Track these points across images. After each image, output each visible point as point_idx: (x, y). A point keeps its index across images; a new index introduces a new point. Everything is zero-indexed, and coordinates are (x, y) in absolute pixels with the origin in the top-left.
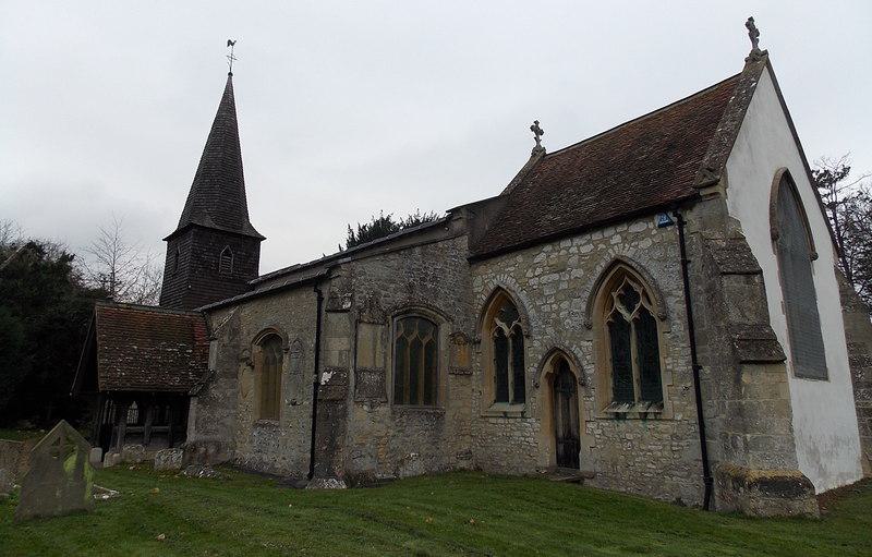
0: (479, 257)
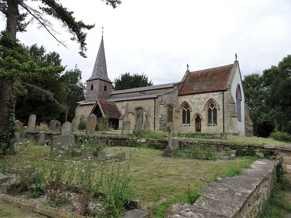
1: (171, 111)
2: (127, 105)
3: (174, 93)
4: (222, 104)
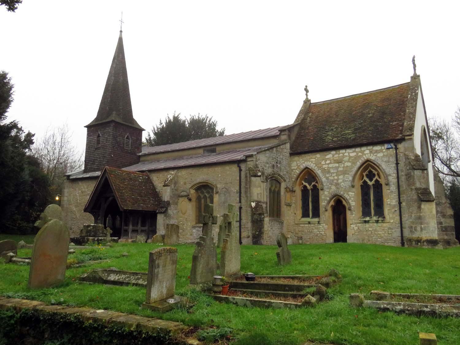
0: (295, 152)
1: (277, 190)
2: (176, 176)
3: (282, 149)
4: (396, 171)
